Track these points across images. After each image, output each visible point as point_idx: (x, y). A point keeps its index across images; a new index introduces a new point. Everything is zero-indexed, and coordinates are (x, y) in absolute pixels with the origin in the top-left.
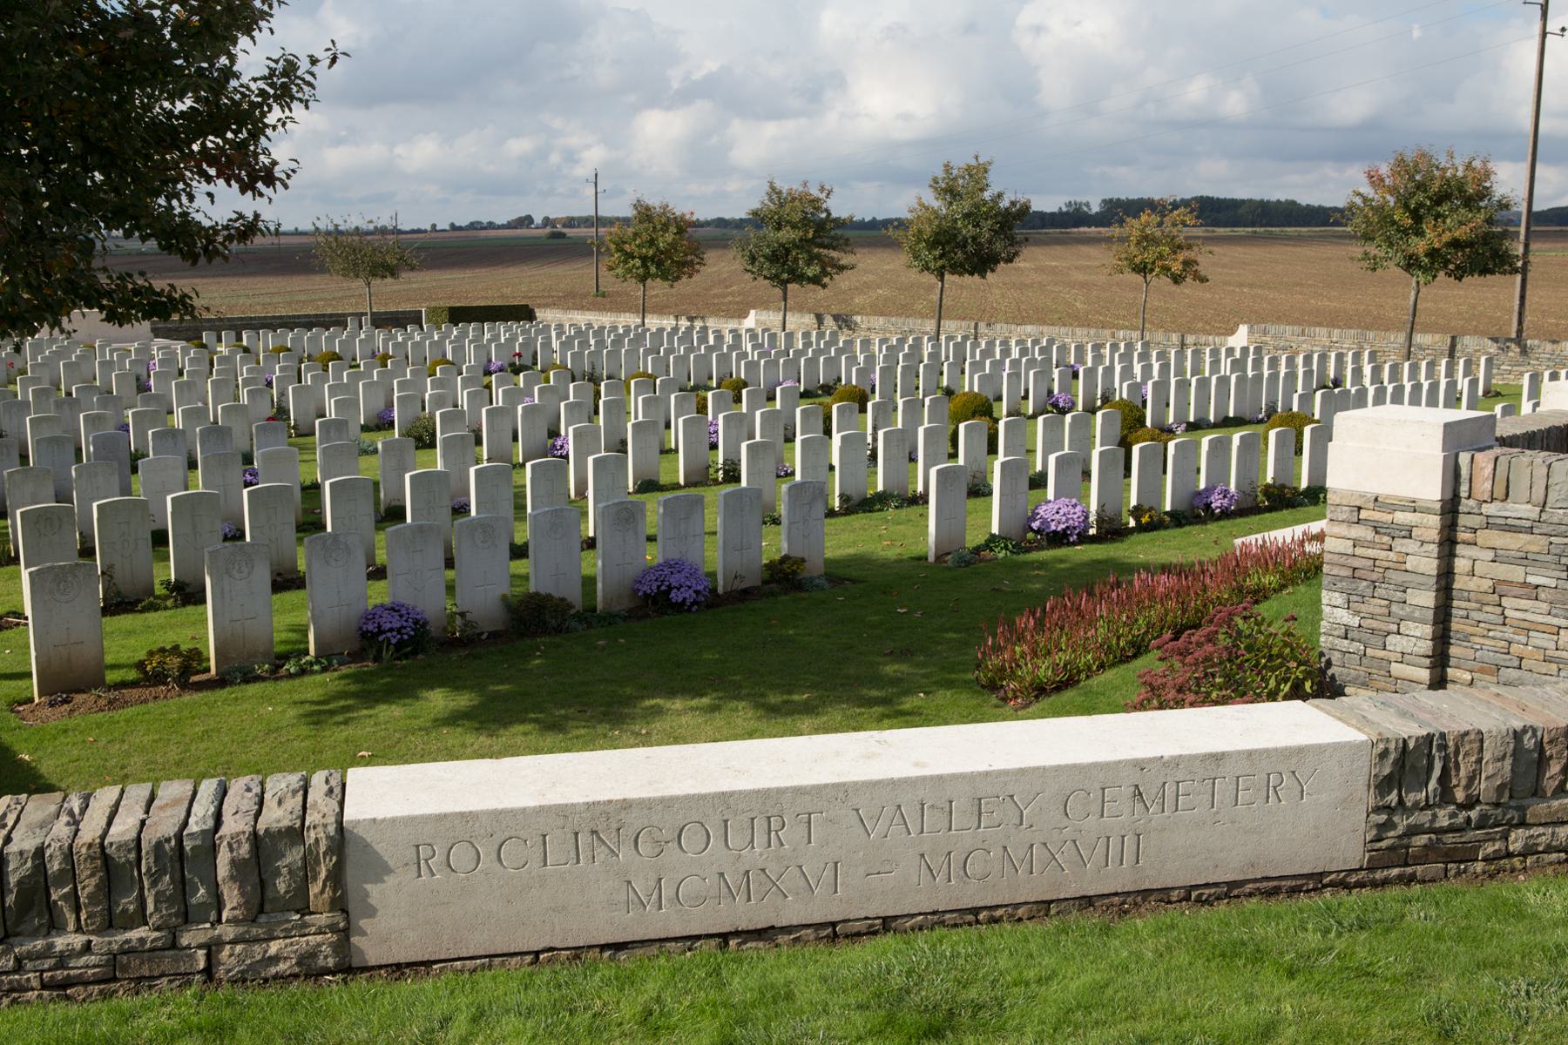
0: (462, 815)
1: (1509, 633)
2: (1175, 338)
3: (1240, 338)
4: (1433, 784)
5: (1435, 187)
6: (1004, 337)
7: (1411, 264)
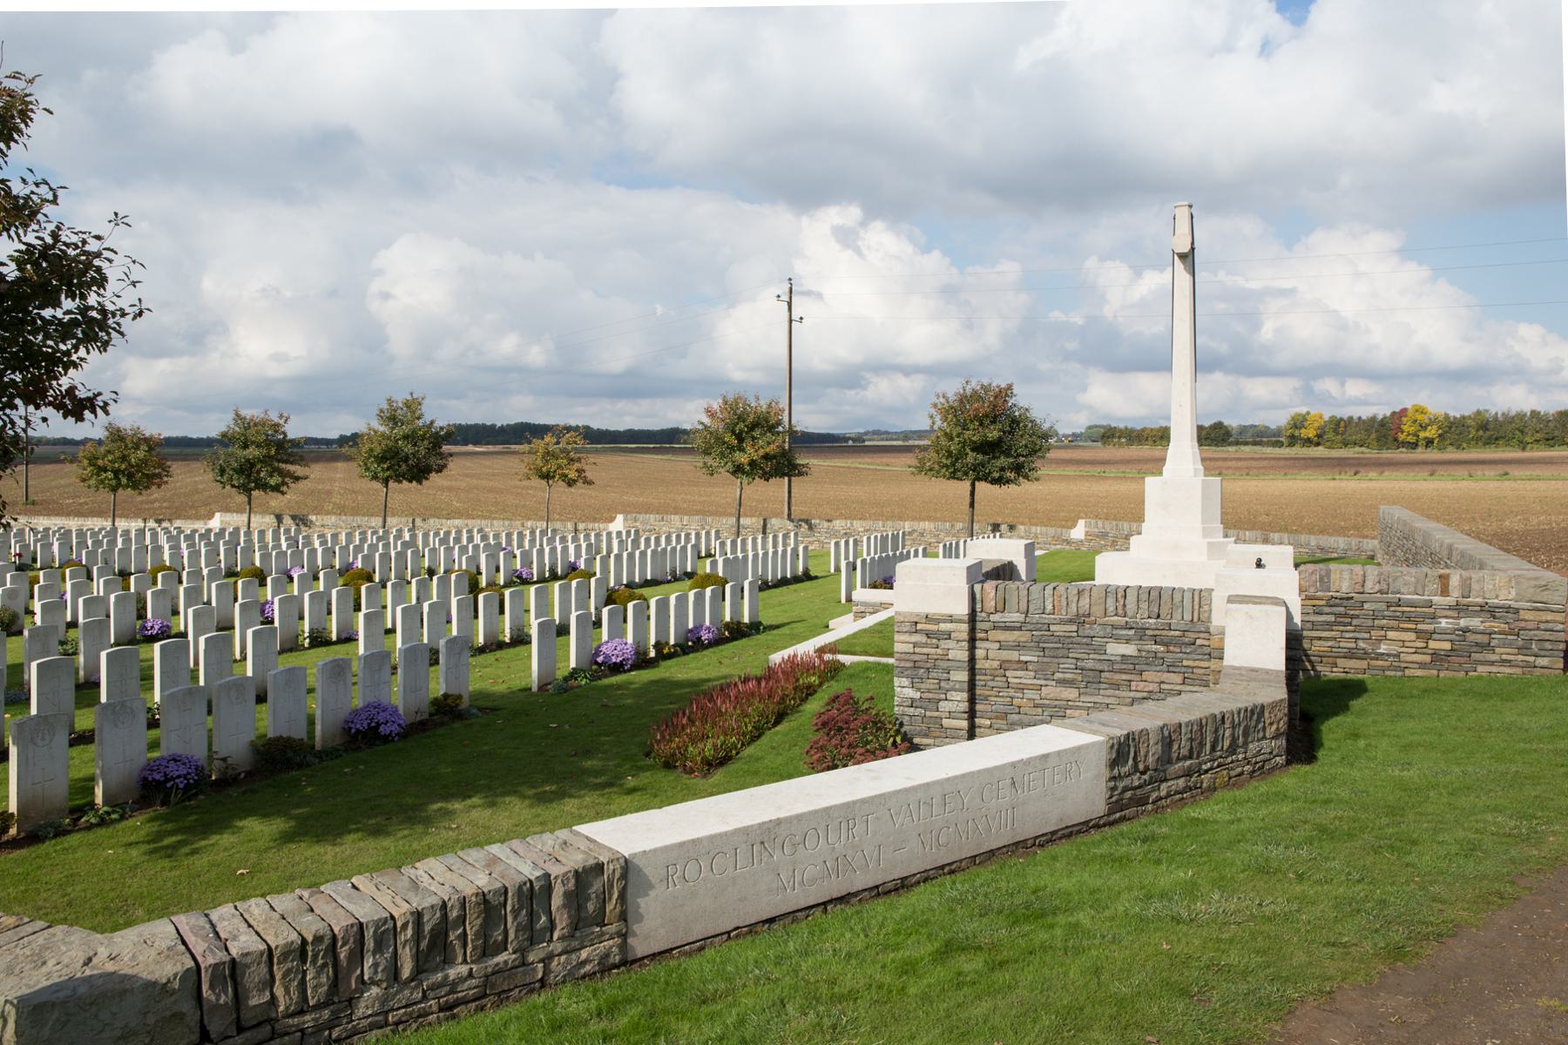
0: (693, 841)
1: (1012, 692)
2: (570, 526)
3: (618, 524)
4: (1131, 762)
5: (751, 419)
6: (452, 529)
7: (738, 470)
